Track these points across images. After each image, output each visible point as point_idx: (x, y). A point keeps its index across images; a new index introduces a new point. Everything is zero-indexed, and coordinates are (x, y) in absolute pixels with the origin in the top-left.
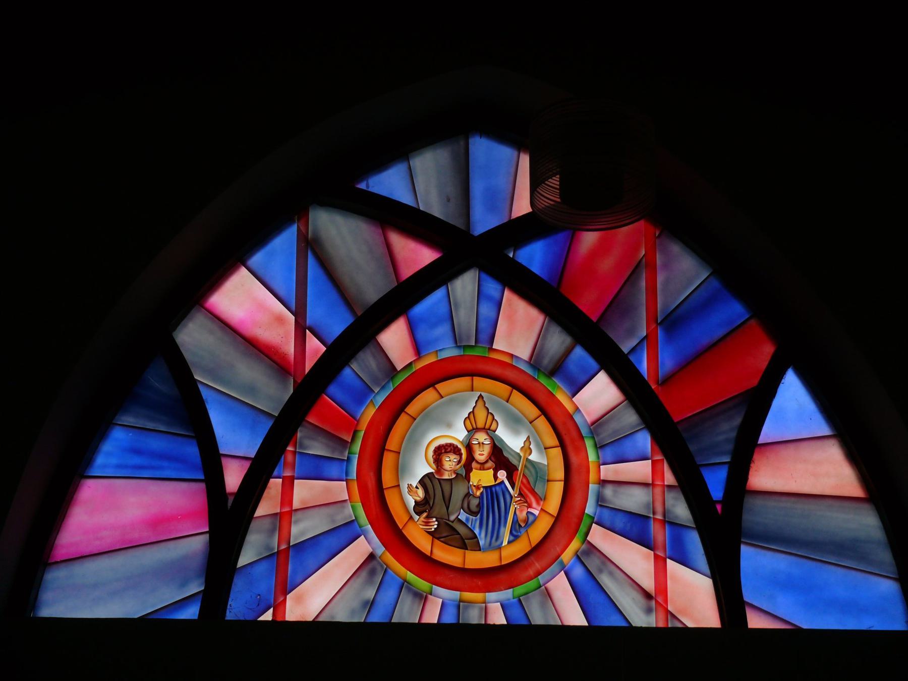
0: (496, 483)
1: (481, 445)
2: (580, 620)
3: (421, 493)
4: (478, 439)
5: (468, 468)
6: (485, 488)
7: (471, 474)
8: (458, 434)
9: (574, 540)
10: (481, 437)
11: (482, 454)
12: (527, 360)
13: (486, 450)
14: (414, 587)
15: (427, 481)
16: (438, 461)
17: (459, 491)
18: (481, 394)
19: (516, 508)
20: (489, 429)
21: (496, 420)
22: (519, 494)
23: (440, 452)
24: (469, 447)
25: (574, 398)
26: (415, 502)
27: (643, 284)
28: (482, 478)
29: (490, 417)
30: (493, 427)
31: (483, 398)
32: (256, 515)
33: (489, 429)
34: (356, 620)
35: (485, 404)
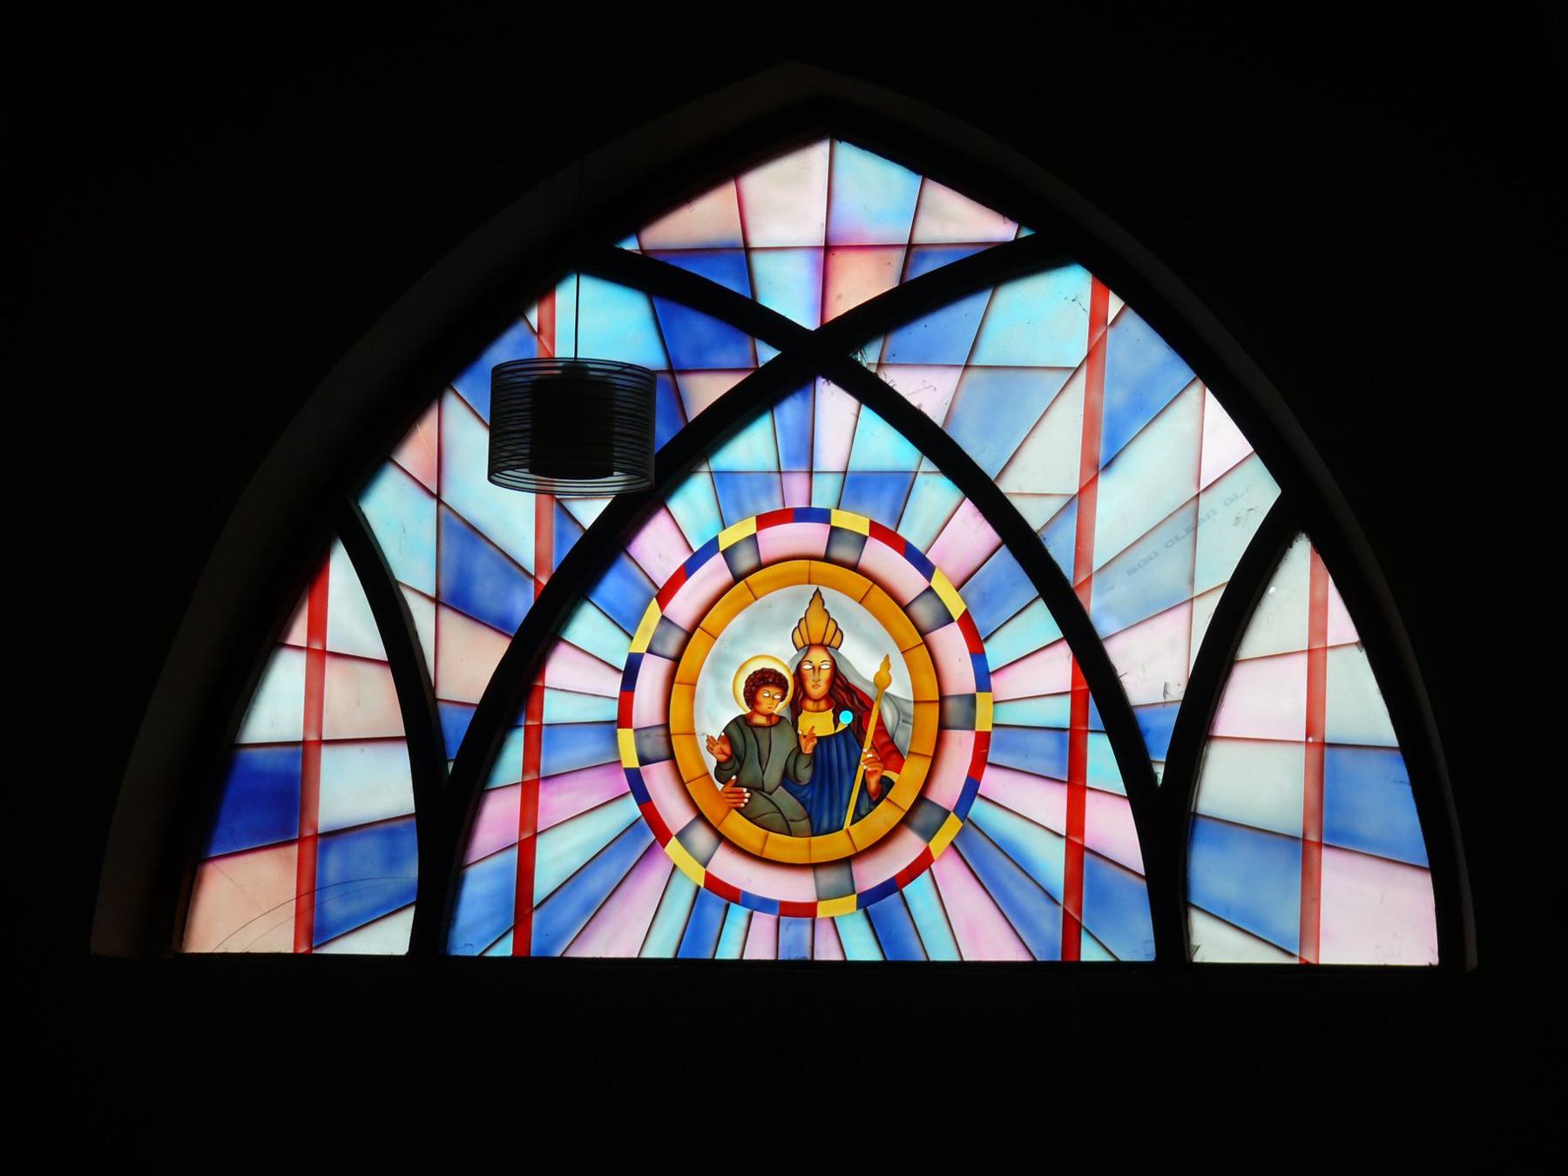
0: (837, 731)
1: (817, 670)
2: (405, 921)
3: (727, 749)
4: (811, 662)
5: (796, 708)
6: (819, 739)
7: (800, 718)
8: (780, 654)
9: (697, 415)
10: (818, 657)
11: (818, 686)
12: (930, 634)
13: (825, 675)
14: (301, 823)
15: (735, 733)
16: (751, 697)
17: (781, 747)
18: (818, 589)
19: (865, 771)
20: (829, 646)
21: (834, 620)
22: (871, 748)
23: (761, 680)
24: (799, 675)
25: (964, 610)
26: (718, 762)
27: (1077, 503)
28: (818, 723)
29: (832, 625)
30: (835, 643)
31: (820, 594)
32: (1022, 957)
33: (829, 646)
34: (1148, 960)
35: (824, 604)
